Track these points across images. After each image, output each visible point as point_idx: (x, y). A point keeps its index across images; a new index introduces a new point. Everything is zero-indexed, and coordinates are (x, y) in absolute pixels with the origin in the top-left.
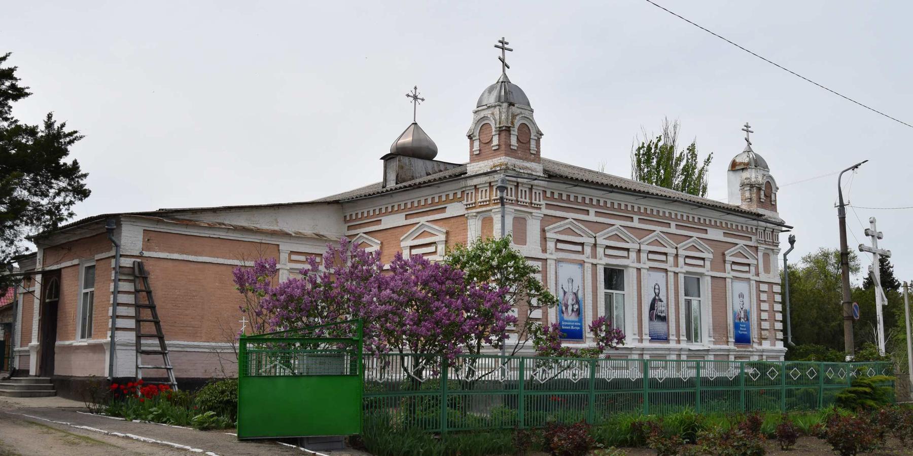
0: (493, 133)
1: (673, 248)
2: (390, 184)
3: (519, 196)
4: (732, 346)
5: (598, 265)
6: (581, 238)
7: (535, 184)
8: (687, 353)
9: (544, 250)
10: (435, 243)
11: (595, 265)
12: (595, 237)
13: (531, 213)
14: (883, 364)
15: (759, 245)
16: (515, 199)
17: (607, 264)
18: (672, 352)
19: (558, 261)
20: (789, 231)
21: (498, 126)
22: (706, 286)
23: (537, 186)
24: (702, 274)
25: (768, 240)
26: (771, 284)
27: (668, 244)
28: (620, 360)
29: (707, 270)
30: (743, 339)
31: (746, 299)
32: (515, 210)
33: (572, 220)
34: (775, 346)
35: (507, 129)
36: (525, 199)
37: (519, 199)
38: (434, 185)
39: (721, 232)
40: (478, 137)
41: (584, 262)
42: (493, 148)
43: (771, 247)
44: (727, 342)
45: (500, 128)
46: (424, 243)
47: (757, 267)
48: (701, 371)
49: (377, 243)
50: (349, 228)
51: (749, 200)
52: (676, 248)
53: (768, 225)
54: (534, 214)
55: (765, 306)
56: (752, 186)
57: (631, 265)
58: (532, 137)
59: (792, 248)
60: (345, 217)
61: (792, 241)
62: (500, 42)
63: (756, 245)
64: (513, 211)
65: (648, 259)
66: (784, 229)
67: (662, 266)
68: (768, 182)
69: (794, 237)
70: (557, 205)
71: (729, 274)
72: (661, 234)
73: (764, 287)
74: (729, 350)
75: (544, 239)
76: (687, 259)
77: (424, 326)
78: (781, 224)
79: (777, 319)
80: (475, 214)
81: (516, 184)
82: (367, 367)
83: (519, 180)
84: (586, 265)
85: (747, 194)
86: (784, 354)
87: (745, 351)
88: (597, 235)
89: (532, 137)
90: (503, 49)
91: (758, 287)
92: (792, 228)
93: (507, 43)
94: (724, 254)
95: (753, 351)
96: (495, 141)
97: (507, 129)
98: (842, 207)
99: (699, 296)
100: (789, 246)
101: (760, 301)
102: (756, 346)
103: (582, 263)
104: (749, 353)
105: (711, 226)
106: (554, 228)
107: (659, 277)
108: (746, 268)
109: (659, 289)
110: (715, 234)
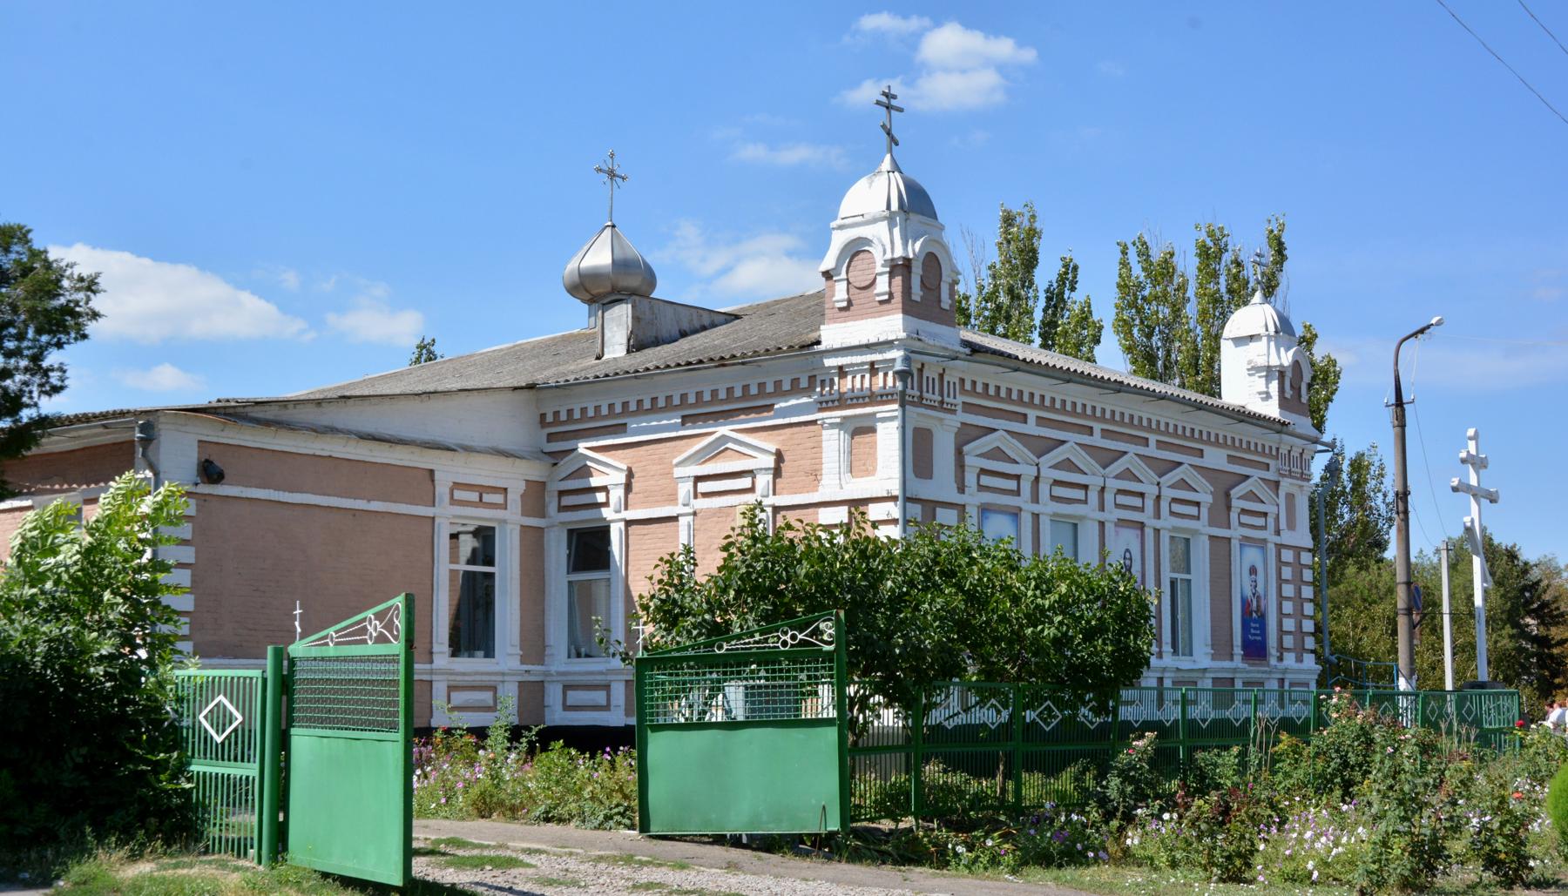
0: (879, 269)
1: (1152, 484)
2: (614, 352)
4: (1238, 662)
6: (1195, 493)
9: (961, 490)
10: (751, 472)
12: (1037, 465)
15: (1281, 479)
16: (919, 394)
18: (506, 678)
19: (985, 510)
21: (889, 256)
24: (1196, 532)
25: (929, 396)
26: (1298, 550)
29: (1203, 527)
30: (1255, 650)
31: (1260, 578)
32: (918, 414)
33: (1189, 468)
34: (1301, 661)
36: (933, 393)
38: (750, 362)
39: (1223, 453)
40: (843, 275)
42: (878, 299)
44: (1231, 658)
45: (892, 260)
46: (711, 473)
48: (1189, 709)
49: (620, 470)
50: (551, 438)
52: (1158, 484)
54: (947, 422)
60: (543, 416)
62: (884, 94)
65: (1170, 511)
66: (1320, 447)
67: (1136, 516)
70: (980, 406)
71: (1236, 533)
72: (1078, 448)
74: (1235, 670)
75: (960, 466)
76: (1173, 505)
77: (1135, 643)
79: (1306, 613)
80: (838, 420)
84: (1023, 514)
86: (1316, 677)
90: (887, 108)
91: (1279, 555)
94: (1228, 495)
96: (882, 285)
98: (1399, 403)
99: (1188, 572)
101: (1281, 581)
103: (1015, 514)
104: (1264, 676)
107: (1130, 538)
108: (1260, 521)
109: (1131, 559)
110: (1215, 458)
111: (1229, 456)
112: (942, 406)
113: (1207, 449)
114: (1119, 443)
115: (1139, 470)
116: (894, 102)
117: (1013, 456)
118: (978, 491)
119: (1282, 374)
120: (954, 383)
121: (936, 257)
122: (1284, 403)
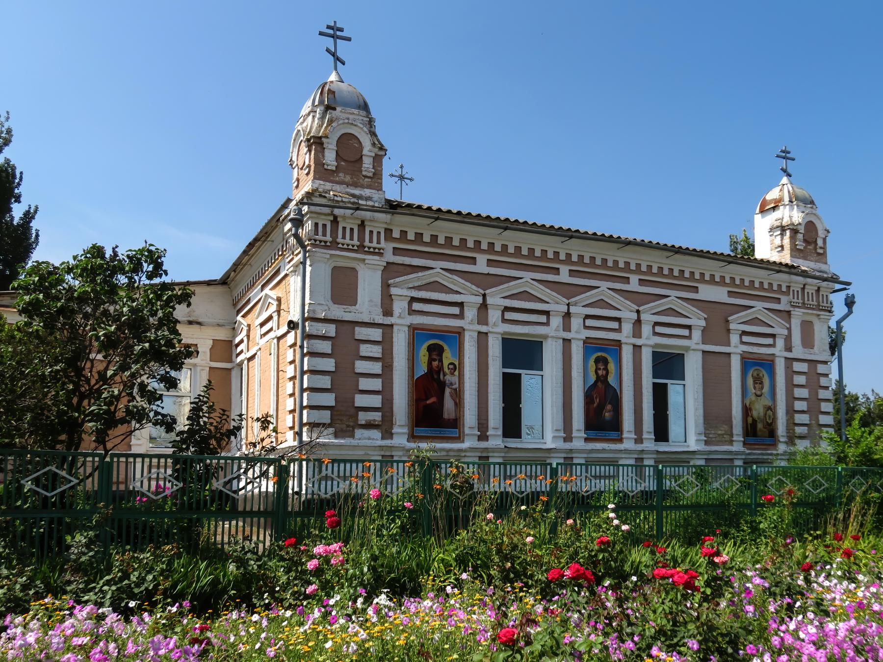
1: (631, 311)
3: (806, 299)
5: (643, 347)
7: (368, 218)
8: (654, 456)
9: (388, 312)
11: (637, 348)
13: (364, 260)
14: (809, 479)
17: (505, 333)
20: (845, 289)
22: (693, 366)
23: (371, 220)
27: (692, 314)
28: (679, 467)
33: (441, 271)
35: (318, 141)
37: (806, 302)
41: (464, 330)
43: (815, 312)
47: (788, 339)
51: (780, 249)
53: (809, 280)
54: (367, 261)
55: (799, 393)
56: (783, 229)
57: (694, 347)
58: (364, 153)
59: (850, 312)
61: (850, 303)
63: (787, 309)
64: (801, 314)
66: (838, 286)
68: (811, 222)
69: (853, 296)
70: (415, 250)
73: (798, 367)
78: (834, 279)
81: (332, 218)
82: (291, 474)
83: (337, 211)
84: (624, 347)
85: (778, 241)
87: (762, 454)
88: (487, 292)
89: (365, 152)
92: (849, 284)
93: (789, 153)
95: (778, 454)
97: (318, 141)
100: (846, 310)
102: (782, 448)
105: (702, 279)
106: (652, 308)
111: (729, 292)
112: (361, 248)
113: (701, 287)
114: (591, 281)
115: (681, 308)
116: (788, 155)
117: (455, 288)
118: (409, 314)
119: (795, 232)
120: (798, 291)
121: (339, 139)
122: (795, 251)
